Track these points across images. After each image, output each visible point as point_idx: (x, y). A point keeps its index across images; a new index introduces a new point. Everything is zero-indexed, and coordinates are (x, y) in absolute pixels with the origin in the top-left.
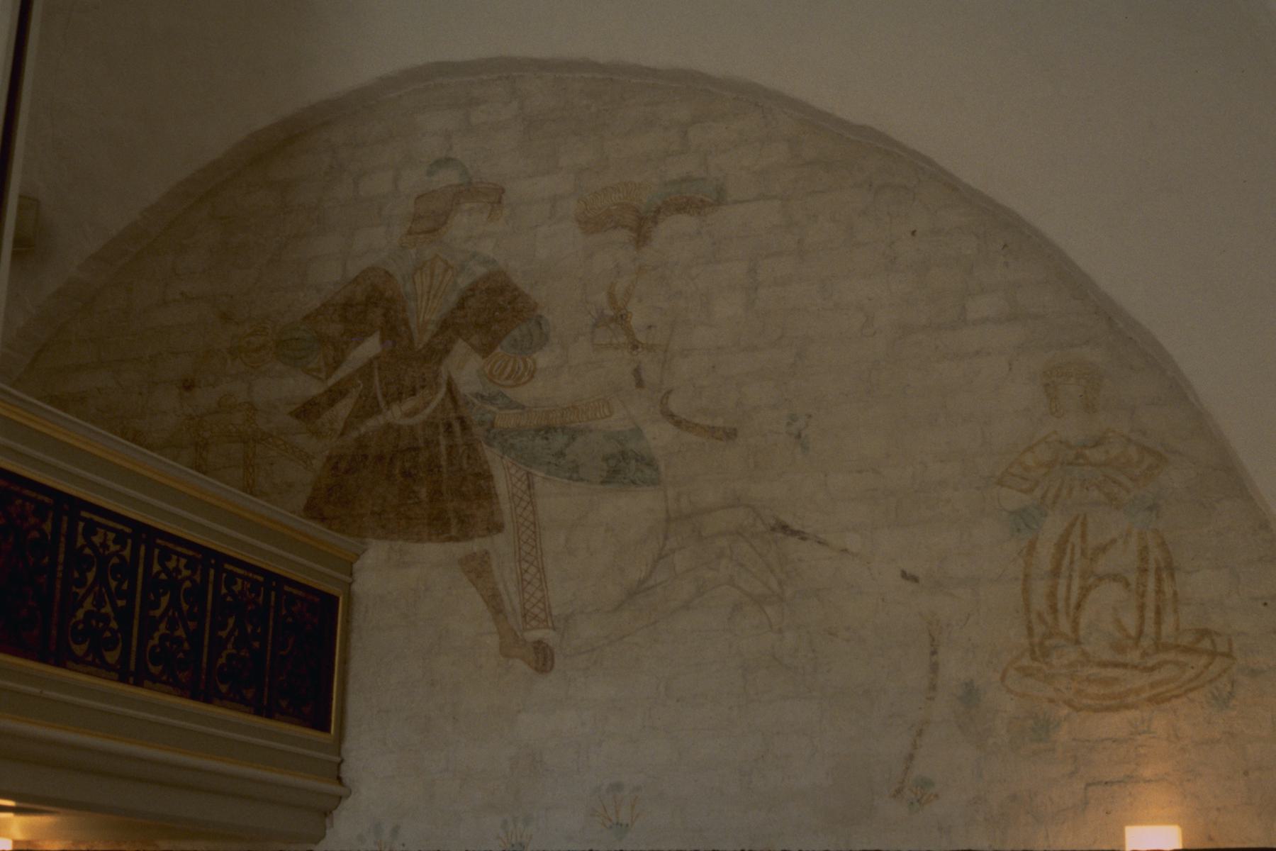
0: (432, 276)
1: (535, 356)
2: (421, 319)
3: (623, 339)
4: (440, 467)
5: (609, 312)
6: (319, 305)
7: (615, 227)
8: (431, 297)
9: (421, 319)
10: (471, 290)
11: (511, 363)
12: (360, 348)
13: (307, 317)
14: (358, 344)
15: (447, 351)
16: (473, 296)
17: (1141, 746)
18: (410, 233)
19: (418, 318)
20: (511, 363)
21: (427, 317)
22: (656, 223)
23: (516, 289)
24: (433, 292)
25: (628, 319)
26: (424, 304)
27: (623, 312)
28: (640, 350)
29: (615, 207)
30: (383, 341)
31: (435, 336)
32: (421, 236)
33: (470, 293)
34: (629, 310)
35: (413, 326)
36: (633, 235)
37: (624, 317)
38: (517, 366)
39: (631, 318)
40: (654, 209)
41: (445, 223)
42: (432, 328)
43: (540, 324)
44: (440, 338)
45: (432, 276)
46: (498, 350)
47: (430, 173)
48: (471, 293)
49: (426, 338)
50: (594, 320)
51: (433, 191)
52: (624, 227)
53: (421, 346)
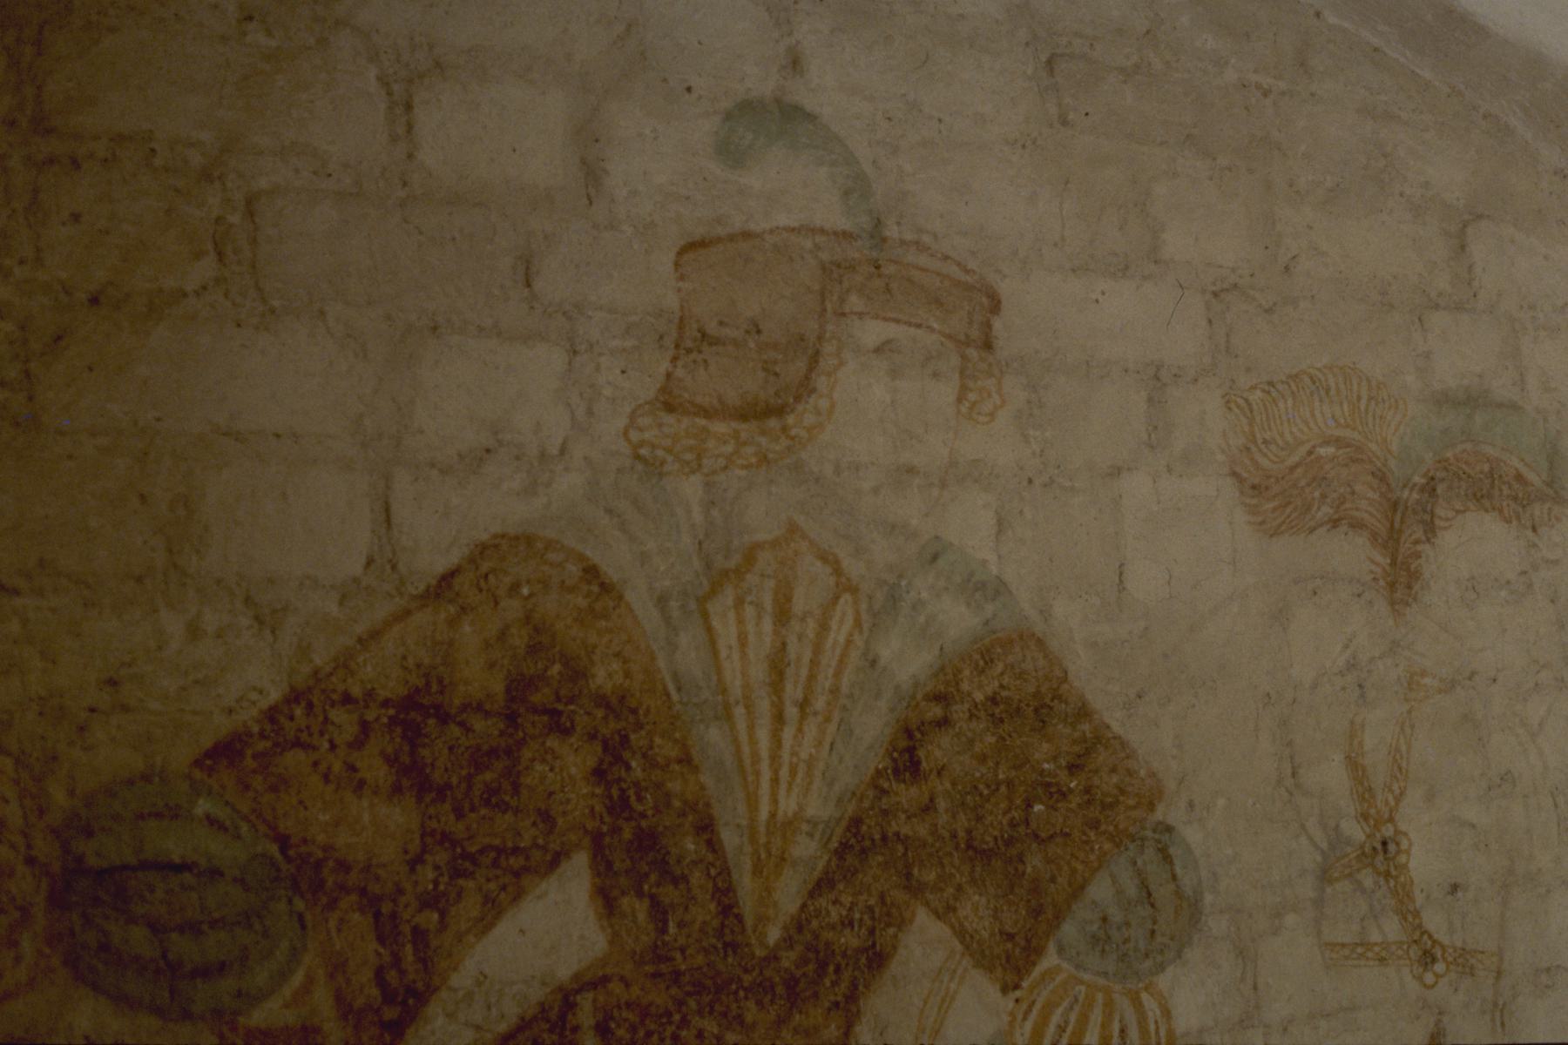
0: (783, 615)
1: (1163, 982)
2: (764, 814)
3: (1392, 929)
4: (1054, 979)
5: (1355, 832)
6: (275, 695)
7: (1335, 523)
8: (792, 712)
9: (764, 814)
10: (938, 698)
11: (1096, 1016)
12: (505, 929)
13: (226, 751)
14: (492, 911)
15: (877, 959)
16: (944, 723)
17: (981, 795)
18: (668, 401)
19: (752, 803)
20: (1096, 1016)
21: (788, 805)
22: (1430, 530)
23: (1084, 712)
24: (792, 691)
25: (1403, 859)
26: (763, 736)
27: (1388, 831)
28: (1440, 967)
29: (1330, 450)
30: (606, 900)
31: (823, 884)
32: (720, 427)
33: (936, 711)
34: (1403, 827)
35: (729, 838)
36: (1379, 559)
37: (1392, 847)
38: (1116, 1027)
39: (1408, 852)
40: (1418, 480)
41: (805, 388)
42: (808, 850)
43: (1167, 859)
44: (847, 900)
45: (783, 615)
46: (1050, 960)
47: (731, 153)
48: (936, 711)
49: (789, 894)
50: (1319, 859)
51: (747, 235)
52: (1357, 525)
53: (774, 934)
